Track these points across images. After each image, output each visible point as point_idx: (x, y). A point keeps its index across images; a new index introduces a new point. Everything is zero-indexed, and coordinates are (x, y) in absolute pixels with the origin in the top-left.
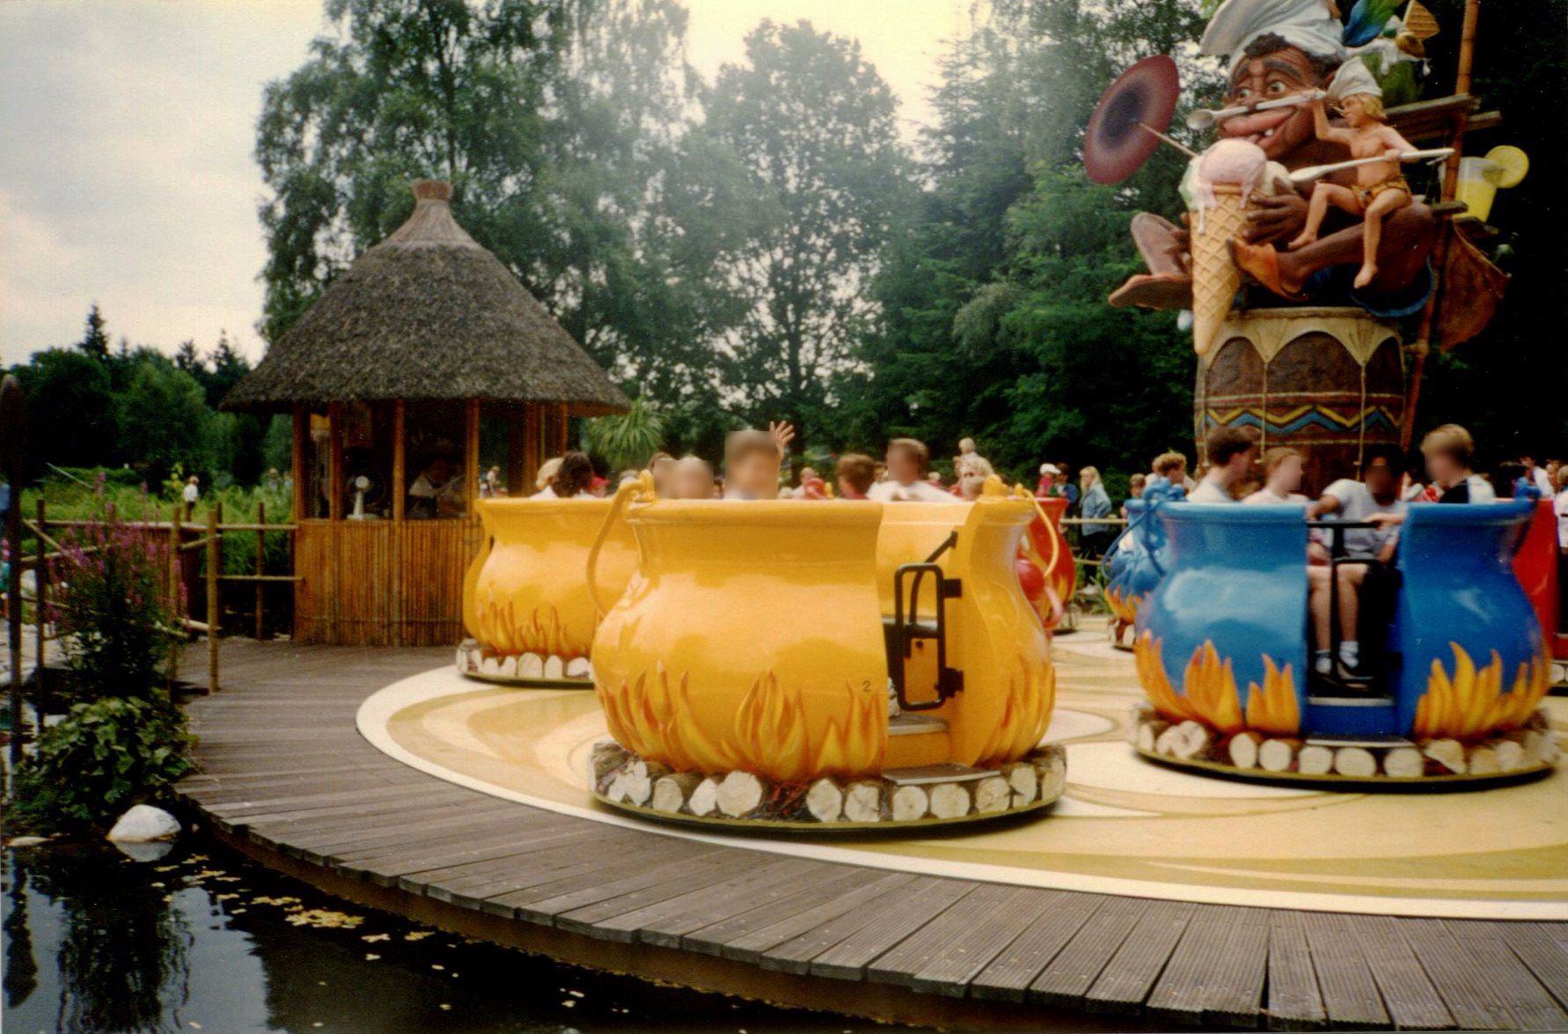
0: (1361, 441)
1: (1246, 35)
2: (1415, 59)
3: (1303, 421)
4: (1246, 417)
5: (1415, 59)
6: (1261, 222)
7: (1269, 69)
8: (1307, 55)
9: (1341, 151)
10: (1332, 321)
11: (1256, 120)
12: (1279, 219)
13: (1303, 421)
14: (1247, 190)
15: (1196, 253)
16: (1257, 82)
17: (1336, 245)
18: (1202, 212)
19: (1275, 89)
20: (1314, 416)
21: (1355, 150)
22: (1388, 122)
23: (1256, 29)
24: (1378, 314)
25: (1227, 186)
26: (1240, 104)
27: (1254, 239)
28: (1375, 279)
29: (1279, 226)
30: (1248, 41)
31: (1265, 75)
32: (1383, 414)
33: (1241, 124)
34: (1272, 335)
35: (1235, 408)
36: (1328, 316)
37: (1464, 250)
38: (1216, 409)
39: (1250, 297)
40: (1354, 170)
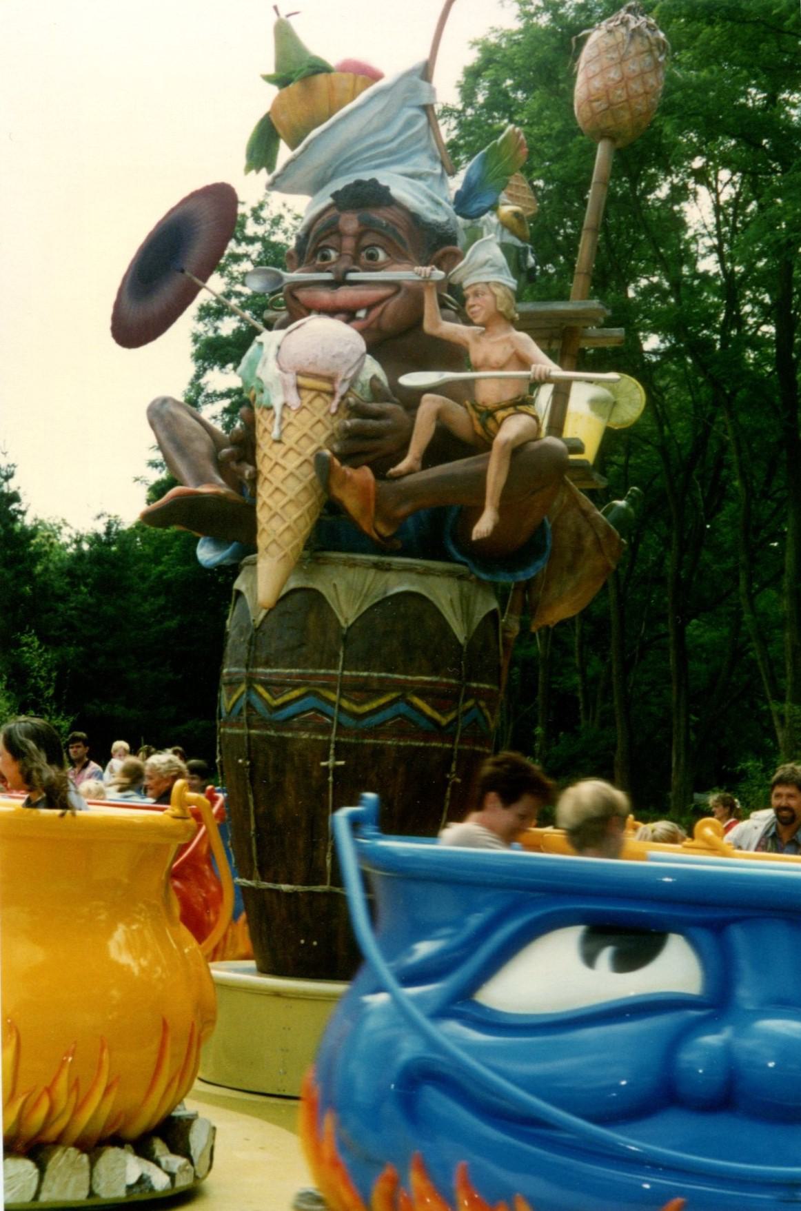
0: (333, 737)
1: (333, 177)
2: (518, 243)
3: (389, 713)
4: (311, 702)
5: (518, 243)
6: (351, 435)
7: (367, 227)
8: (414, 218)
9: (453, 355)
10: (433, 581)
11: (345, 295)
12: (378, 435)
13: (389, 713)
14: (341, 390)
15: (264, 466)
16: (349, 243)
17: (450, 479)
18: (278, 409)
19: (372, 257)
20: (402, 708)
21: (476, 354)
22: (525, 323)
23: (348, 171)
24: (484, 576)
25: (314, 381)
26: (320, 270)
27: (348, 457)
28: (497, 528)
29: (377, 443)
30: (339, 184)
31: (359, 236)
32: (480, 709)
33: (324, 296)
34: (350, 590)
35: (296, 686)
36: (427, 572)
37: (574, 501)
38: (265, 684)
39: (330, 533)
40: (469, 385)
